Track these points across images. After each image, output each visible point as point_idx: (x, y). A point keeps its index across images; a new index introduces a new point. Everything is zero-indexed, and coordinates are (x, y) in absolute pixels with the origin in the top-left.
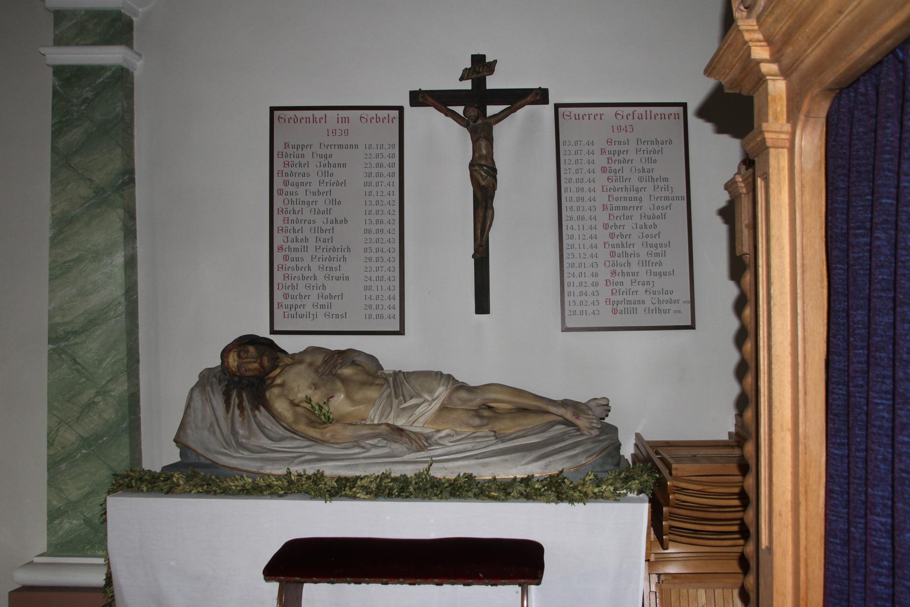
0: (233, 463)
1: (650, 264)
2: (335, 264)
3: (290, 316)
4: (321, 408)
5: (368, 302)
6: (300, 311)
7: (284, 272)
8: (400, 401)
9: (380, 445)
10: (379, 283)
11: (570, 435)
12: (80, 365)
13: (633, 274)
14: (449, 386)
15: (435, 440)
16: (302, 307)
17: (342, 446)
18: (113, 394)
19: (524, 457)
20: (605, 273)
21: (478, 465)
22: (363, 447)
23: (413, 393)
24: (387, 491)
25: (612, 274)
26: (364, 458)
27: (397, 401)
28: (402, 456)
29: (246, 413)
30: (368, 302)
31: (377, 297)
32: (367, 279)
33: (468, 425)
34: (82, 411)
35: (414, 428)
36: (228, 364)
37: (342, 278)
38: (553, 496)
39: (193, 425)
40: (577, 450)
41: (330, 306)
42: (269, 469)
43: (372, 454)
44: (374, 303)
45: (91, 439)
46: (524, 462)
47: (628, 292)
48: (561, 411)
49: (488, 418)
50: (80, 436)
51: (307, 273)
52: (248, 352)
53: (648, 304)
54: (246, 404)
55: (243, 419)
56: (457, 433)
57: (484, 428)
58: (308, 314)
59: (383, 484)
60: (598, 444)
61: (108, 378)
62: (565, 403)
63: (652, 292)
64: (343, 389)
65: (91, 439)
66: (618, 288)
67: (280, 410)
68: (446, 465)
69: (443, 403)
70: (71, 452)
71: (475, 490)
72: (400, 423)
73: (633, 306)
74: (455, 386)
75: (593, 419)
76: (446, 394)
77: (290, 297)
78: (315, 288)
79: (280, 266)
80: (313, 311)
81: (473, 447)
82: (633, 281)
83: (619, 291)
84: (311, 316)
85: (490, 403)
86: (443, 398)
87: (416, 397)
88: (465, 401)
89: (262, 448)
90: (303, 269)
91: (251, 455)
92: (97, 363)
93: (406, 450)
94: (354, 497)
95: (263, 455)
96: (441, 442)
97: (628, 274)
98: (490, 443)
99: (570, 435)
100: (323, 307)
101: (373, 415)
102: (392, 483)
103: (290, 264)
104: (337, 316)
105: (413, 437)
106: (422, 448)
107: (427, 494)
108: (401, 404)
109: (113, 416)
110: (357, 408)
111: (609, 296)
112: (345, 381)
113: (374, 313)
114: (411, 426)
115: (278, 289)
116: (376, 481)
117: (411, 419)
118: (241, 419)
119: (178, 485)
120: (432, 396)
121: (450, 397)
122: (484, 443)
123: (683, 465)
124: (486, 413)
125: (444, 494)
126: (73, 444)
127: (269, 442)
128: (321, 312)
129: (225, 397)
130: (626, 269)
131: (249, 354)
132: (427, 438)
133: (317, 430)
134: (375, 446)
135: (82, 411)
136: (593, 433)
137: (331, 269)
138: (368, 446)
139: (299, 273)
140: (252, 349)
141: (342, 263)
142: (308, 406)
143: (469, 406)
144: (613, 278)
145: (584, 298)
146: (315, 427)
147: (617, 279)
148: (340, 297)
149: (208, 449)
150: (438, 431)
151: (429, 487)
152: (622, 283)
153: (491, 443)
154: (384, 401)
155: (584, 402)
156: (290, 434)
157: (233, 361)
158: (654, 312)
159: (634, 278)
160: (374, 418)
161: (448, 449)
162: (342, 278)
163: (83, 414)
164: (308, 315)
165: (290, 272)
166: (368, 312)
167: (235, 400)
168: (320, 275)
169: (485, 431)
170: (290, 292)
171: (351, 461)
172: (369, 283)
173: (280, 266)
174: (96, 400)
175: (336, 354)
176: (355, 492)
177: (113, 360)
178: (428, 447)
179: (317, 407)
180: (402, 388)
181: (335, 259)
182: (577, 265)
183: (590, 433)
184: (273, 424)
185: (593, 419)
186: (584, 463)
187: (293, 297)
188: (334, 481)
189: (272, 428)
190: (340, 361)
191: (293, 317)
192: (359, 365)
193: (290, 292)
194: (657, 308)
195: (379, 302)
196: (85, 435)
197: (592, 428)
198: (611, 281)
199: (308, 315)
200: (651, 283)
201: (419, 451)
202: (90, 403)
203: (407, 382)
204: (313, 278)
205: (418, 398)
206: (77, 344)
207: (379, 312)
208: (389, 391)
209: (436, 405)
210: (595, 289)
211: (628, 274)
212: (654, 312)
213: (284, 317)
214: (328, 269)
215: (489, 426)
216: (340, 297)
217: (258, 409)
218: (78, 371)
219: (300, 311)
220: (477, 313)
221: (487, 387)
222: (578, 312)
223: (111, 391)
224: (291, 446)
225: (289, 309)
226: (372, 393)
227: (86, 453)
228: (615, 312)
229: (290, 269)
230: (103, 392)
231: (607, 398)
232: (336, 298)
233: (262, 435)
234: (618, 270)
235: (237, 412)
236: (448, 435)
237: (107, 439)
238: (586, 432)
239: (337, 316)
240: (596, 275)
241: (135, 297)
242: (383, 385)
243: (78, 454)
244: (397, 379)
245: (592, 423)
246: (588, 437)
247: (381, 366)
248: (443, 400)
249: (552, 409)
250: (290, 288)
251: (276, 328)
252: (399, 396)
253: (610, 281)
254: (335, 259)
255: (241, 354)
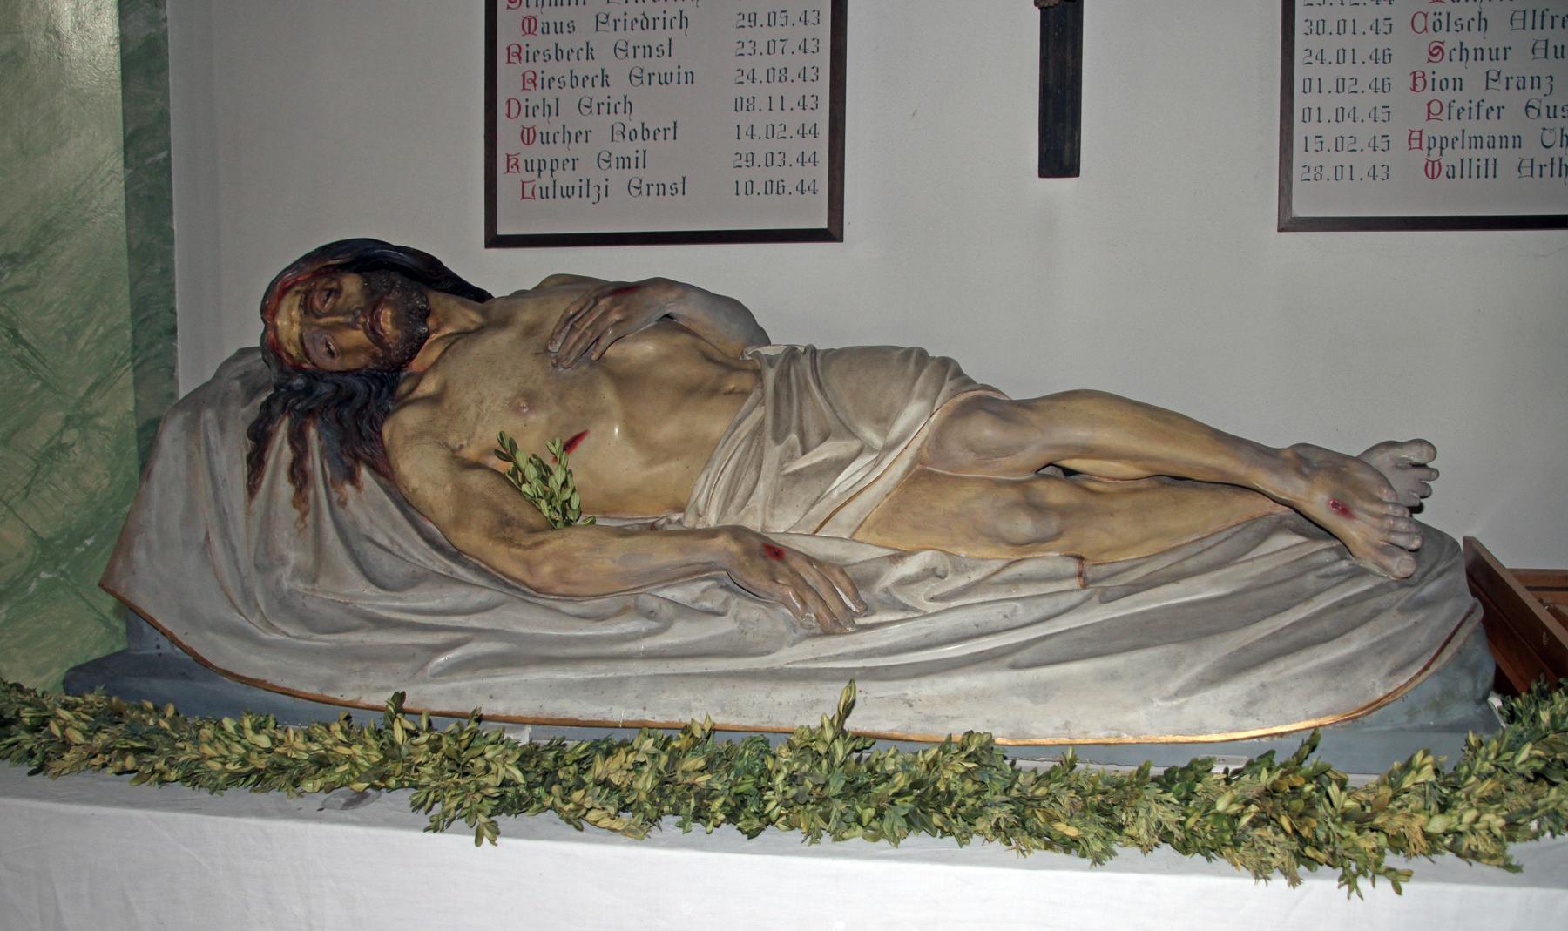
0: (255, 664)
1: (1548, 21)
2: (658, 37)
3: (537, 191)
4: (545, 473)
5: (746, 145)
6: (565, 178)
7: (525, 66)
8: (792, 449)
9: (707, 605)
10: (776, 89)
11: (1322, 572)
12: (26, 344)
13: (1494, 55)
14: (940, 399)
15: (886, 590)
16: (569, 166)
17: (587, 607)
18: (102, 421)
19: (1174, 664)
20: (1410, 51)
21: (1015, 690)
22: (650, 615)
23: (832, 422)
24: (693, 803)
25: (1431, 53)
26: (649, 656)
27: (778, 449)
28: (769, 653)
29: (311, 494)
30: (746, 145)
31: (770, 132)
32: (744, 79)
33: (997, 539)
34: (38, 468)
35: (822, 543)
36: (276, 336)
37: (675, 77)
38: (1280, 847)
39: (154, 536)
40: (1356, 642)
41: (643, 160)
42: (353, 690)
43: (676, 641)
44: (761, 147)
45: (59, 542)
46: (1173, 685)
47: (1475, 111)
48: (1294, 488)
49: (1064, 512)
50: (35, 535)
51: (583, 68)
52: (338, 292)
53: (1531, 149)
54: (315, 463)
55: (304, 514)
56: (959, 568)
57: (1044, 546)
58: (584, 184)
59: (679, 776)
60: (1420, 616)
61: (91, 381)
62: (1303, 460)
63: (1544, 112)
64: (617, 411)
65: (59, 542)
66: (1446, 96)
67: (414, 483)
68: (910, 688)
69: (917, 459)
70: (17, 577)
71: (1001, 813)
72: (783, 525)
73: (1484, 153)
74: (961, 398)
75: (1396, 518)
76: (926, 429)
77: (539, 136)
78: (604, 108)
79: (515, 49)
80: (597, 177)
81: (1005, 617)
82: (1493, 75)
83: (1450, 107)
84: (593, 191)
85: (1071, 458)
86: (917, 443)
87: (839, 437)
88: (986, 454)
89: (350, 612)
90: (573, 56)
91: (309, 639)
92: (64, 338)
93: (783, 628)
94: (576, 821)
95: (342, 637)
96: (904, 599)
97: (1479, 54)
98: (1065, 601)
99: (1322, 572)
100: (623, 162)
101: (703, 497)
102: (707, 777)
103: (539, 42)
104: (661, 189)
105: (810, 581)
106: (837, 622)
107: (828, 822)
108: (792, 458)
109: (106, 482)
110: (660, 469)
111: (1420, 121)
112: (627, 381)
113: (760, 175)
114: (814, 534)
115: (509, 116)
116: (654, 764)
117: (813, 511)
118: (296, 514)
119: (66, 745)
120: (885, 433)
121: (939, 438)
122: (1040, 601)
123: (1530, 605)
124: (1056, 494)
125: (886, 825)
126: (20, 555)
127: (371, 590)
128: (618, 179)
129: (250, 442)
130: (1473, 40)
131: (341, 301)
132: (860, 582)
133: (514, 550)
134: (685, 611)
135: (38, 468)
136: (1395, 567)
137: (648, 52)
138: (667, 610)
139: (559, 69)
140: (352, 285)
141: (677, 33)
142: (504, 466)
143: (1002, 469)
144: (1432, 66)
145: (1346, 127)
146: (509, 542)
147: (1445, 69)
148: (670, 134)
149: (190, 617)
150: (898, 557)
151: (837, 791)
152: (1458, 84)
153: (1070, 604)
154: (745, 442)
155: (1355, 456)
156: (439, 563)
157: (289, 322)
158: (1546, 171)
159: (1496, 65)
160: (706, 506)
161: (920, 628)
162: (675, 77)
163: (39, 477)
164: (585, 189)
165: (538, 66)
166: (744, 175)
167: (280, 451)
168: (618, 70)
169: (1048, 560)
170: (540, 123)
171: (602, 666)
172: (747, 90)
173: (515, 49)
174: (65, 440)
175: (604, 297)
176: (579, 806)
177: (101, 330)
178: (858, 615)
179: (531, 472)
180: (800, 404)
181: (659, 24)
182: (1331, 26)
183: (1385, 569)
184: (395, 527)
185: (1396, 518)
186: (1381, 695)
187: (546, 139)
188: (510, 761)
189: (392, 540)
190: (617, 317)
191: (544, 195)
192: (685, 330)
193: (540, 123)
194: (1557, 162)
195: (774, 145)
196: (47, 534)
197: (1391, 549)
198: (1429, 79)
199: (585, 189)
200: (1545, 83)
201: (827, 633)
202: (52, 448)
203: (820, 386)
204: (598, 81)
205: (843, 438)
206: (18, 288)
207: (774, 174)
208: (758, 413)
209: (897, 466)
210: (1380, 99)
211: (1479, 54)
212: (1546, 171)
213: (523, 197)
214: (640, 52)
215: (1062, 542)
216: (670, 134)
217: (352, 478)
218: (23, 362)
219: (565, 178)
220: (1042, 174)
221: (1062, 404)
222: (1328, 172)
223: (98, 414)
224: (435, 604)
225: (536, 173)
226: (712, 422)
227: (49, 579)
228: (1432, 171)
229: (540, 58)
230: (80, 419)
231: (1433, 447)
232: (660, 136)
233: (351, 570)
234: (1451, 40)
235: (286, 489)
236: (931, 573)
237: (92, 544)
238: (1368, 564)
239: (661, 189)
240: (1386, 57)
241: (163, 154)
242: (745, 394)
243: (31, 581)
244: (792, 371)
245: (1392, 531)
246: (1379, 580)
247: (761, 331)
248: (919, 449)
249: (1264, 479)
250: (539, 112)
251: (503, 230)
252: (788, 432)
253: (1423, 76)
254: (659, 24)
255: (317, 303)
